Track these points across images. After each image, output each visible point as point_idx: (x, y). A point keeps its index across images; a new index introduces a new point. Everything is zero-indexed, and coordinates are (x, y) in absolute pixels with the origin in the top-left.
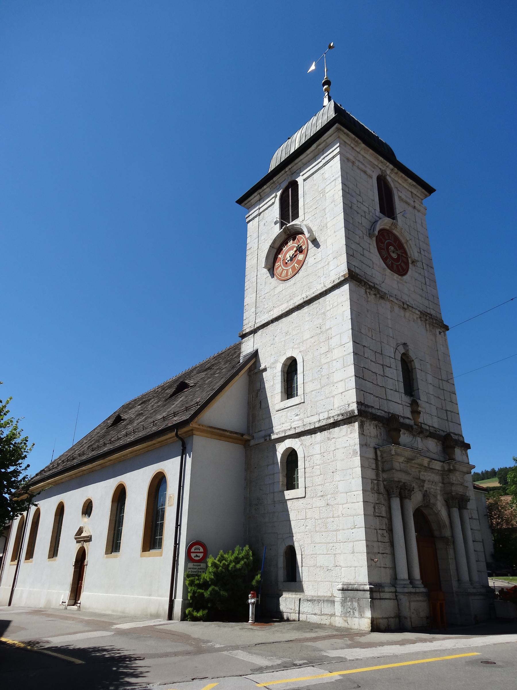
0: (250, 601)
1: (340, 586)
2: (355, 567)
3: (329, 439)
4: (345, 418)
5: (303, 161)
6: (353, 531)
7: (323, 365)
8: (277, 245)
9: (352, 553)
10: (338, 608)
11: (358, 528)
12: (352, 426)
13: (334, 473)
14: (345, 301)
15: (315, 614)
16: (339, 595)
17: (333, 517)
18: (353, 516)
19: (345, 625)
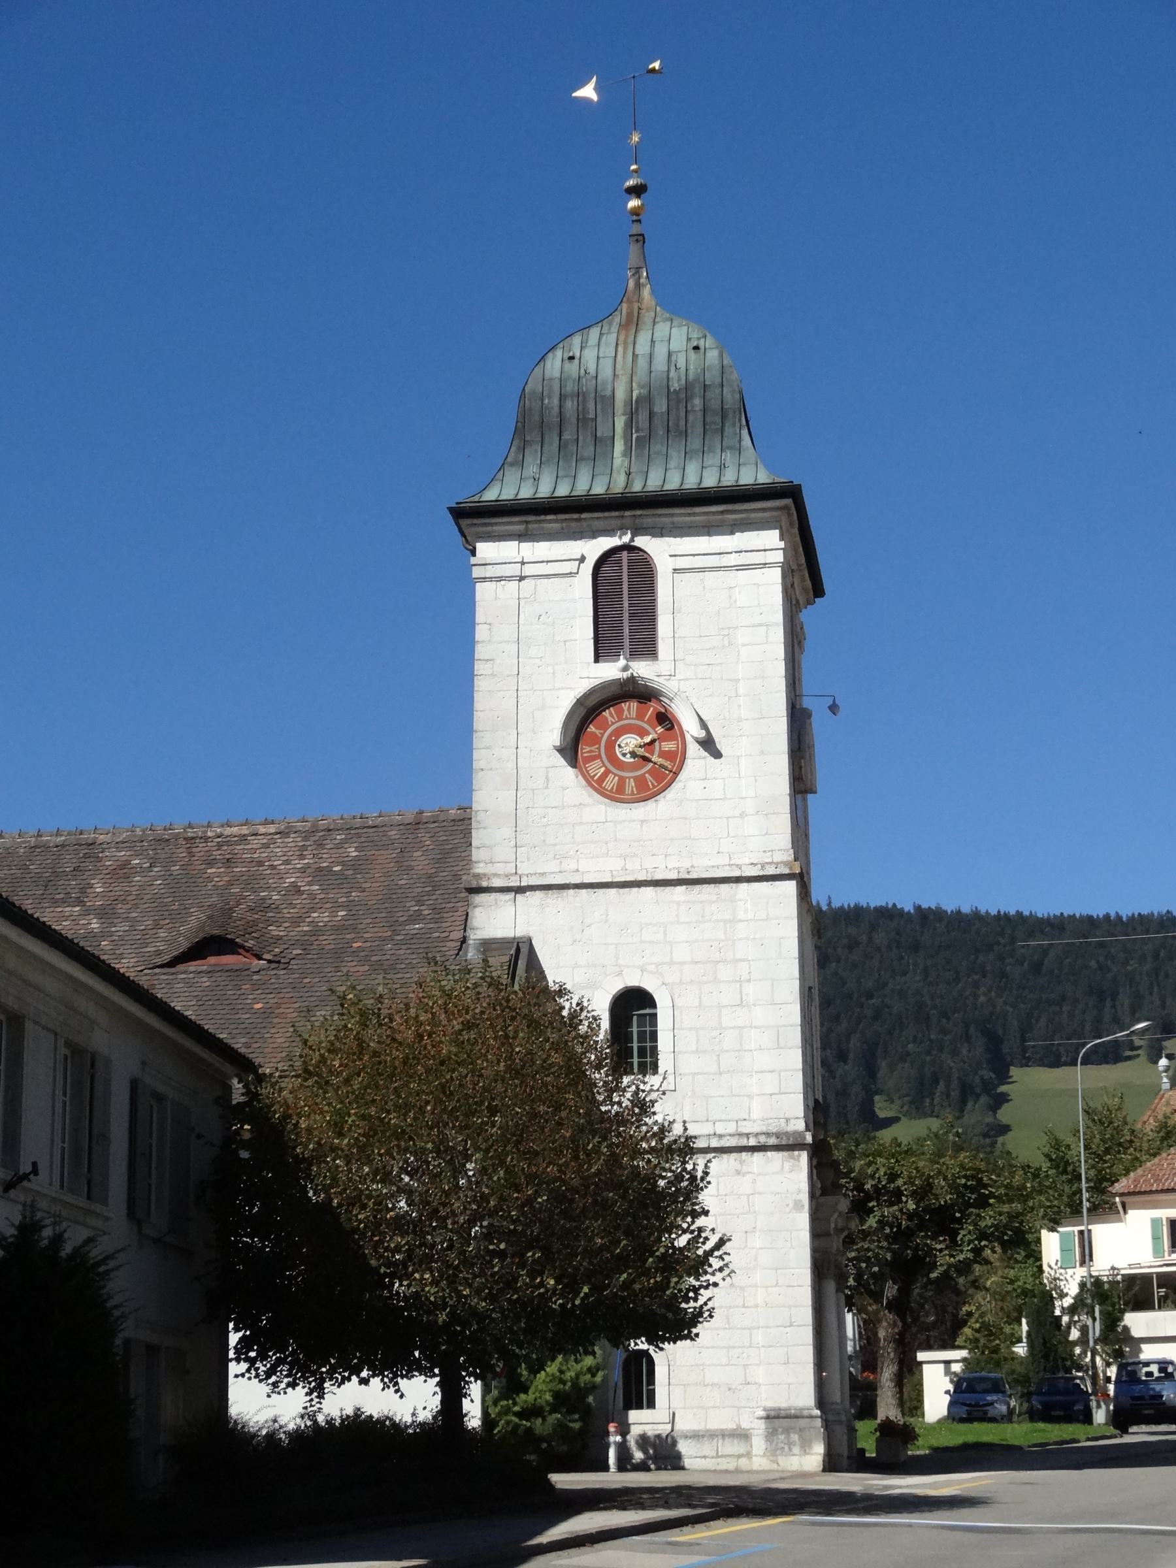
0: (612, 1439)
1: (763, 1414)
2: (789, 1384)
3: (738, 1173)
4: (784, 1143)
5: (676, 519)
6: (788, 1329)
7: (725, 1029)
8: (592, 702)
9: (784, 1364)
10: (759, 1444)
11: (798, 1326)
12: (792, 1157)
13: (749, 1235)
14: (786, 918)
15: (705, 1457)
16: (759, 1428)
17: (744, 1306)
18: (790, 1307)
19: (774, 1466)
